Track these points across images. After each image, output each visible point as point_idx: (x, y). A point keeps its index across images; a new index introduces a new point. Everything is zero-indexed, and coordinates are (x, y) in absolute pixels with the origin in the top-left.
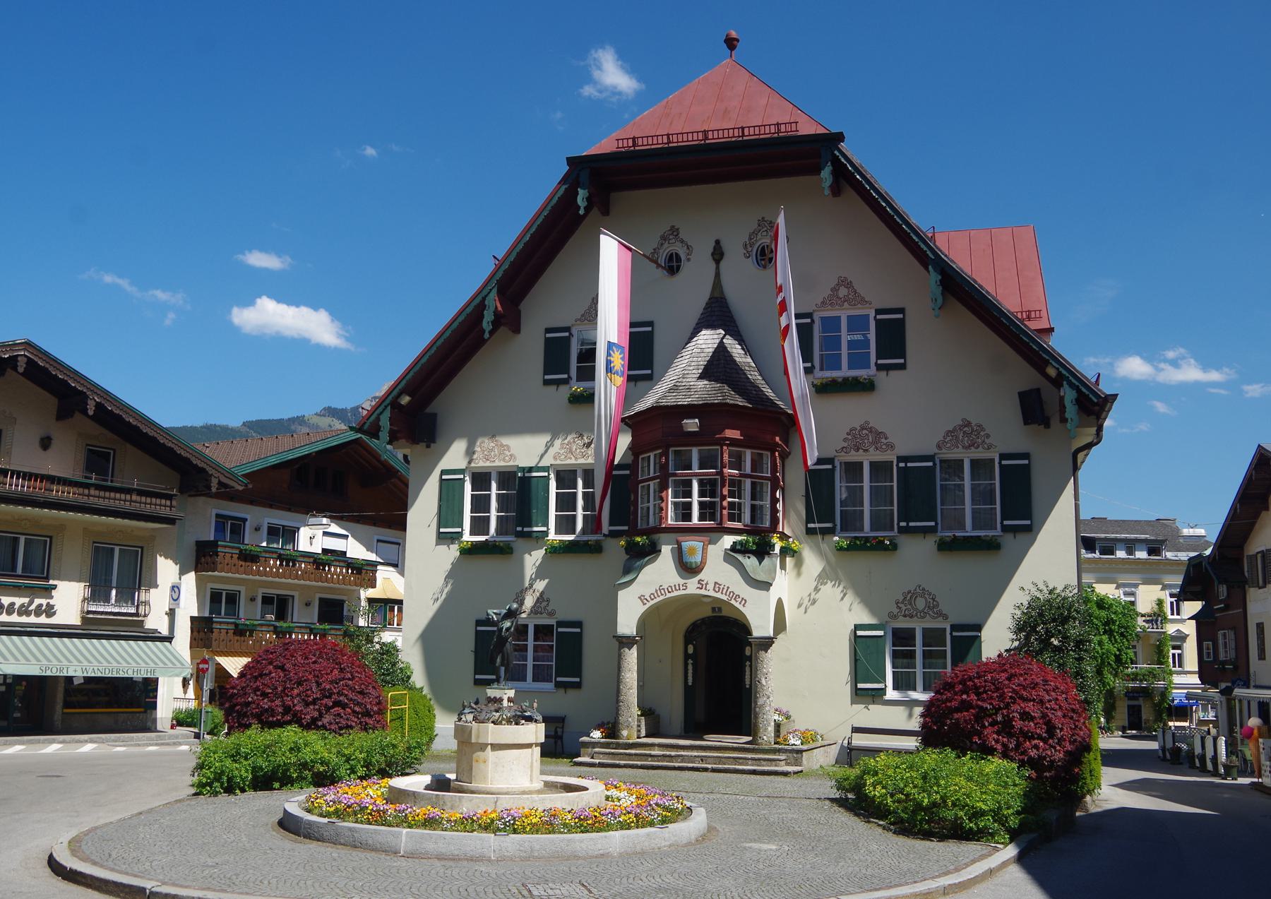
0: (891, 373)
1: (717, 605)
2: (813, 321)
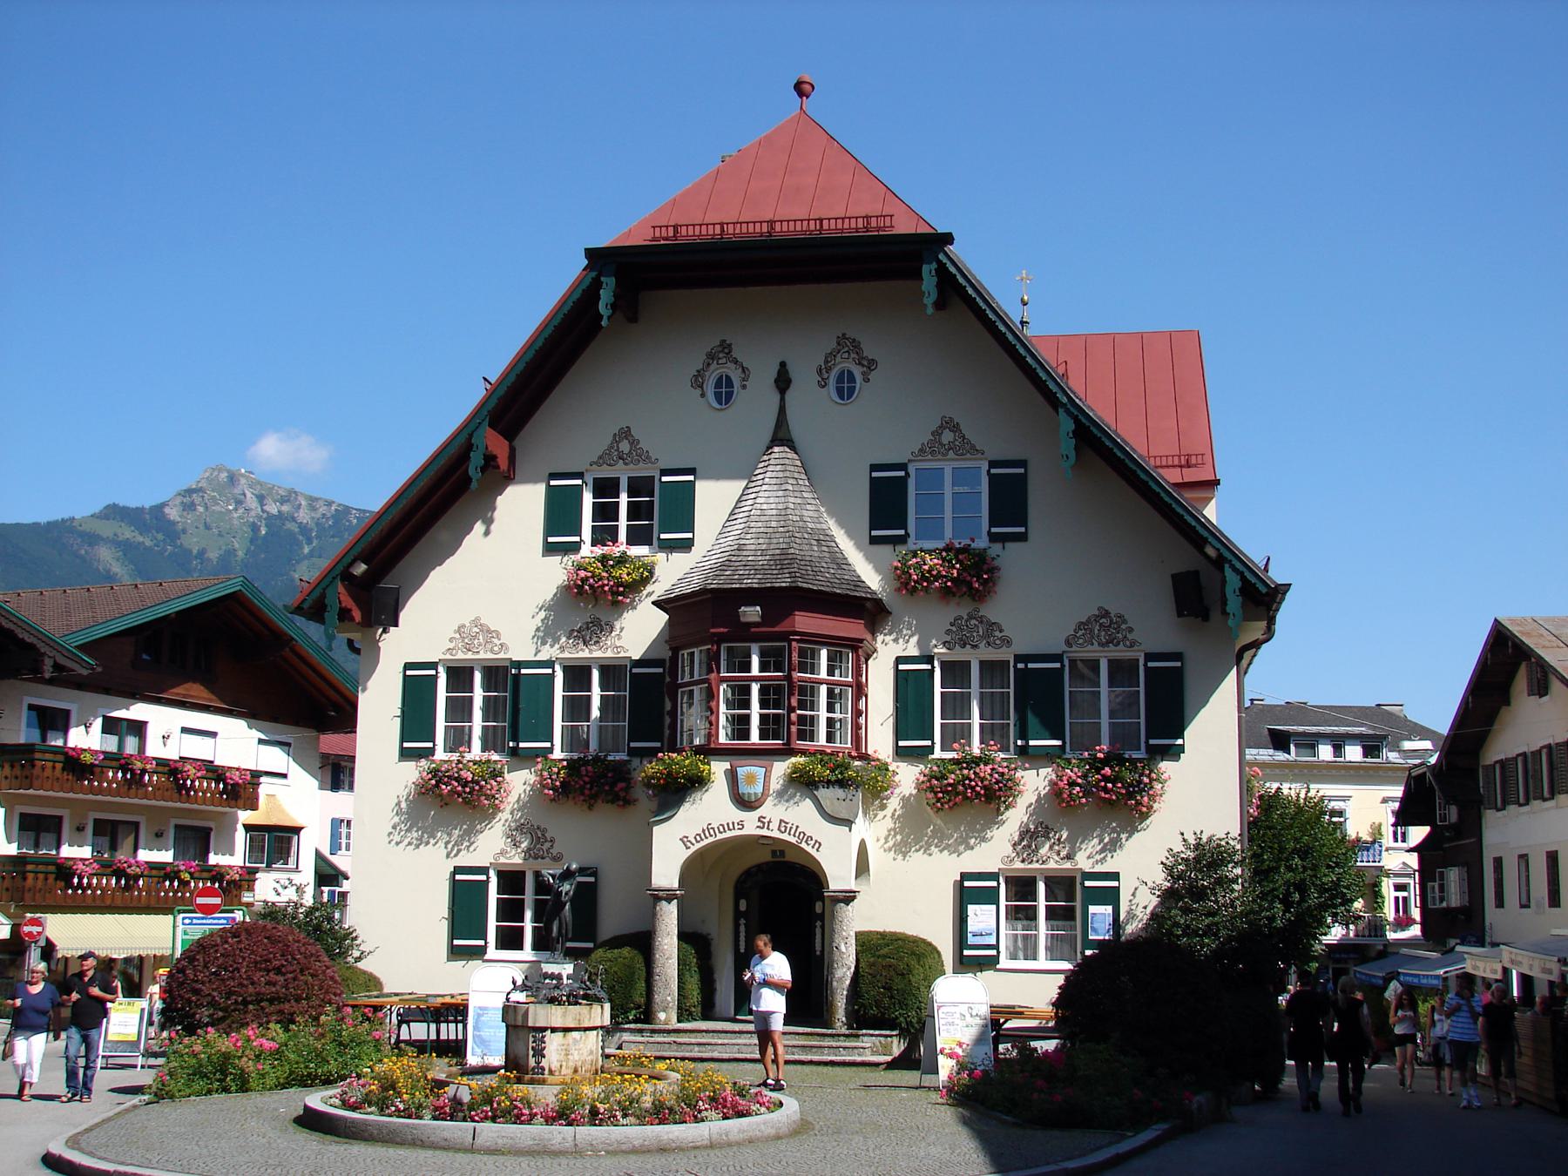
0: (1009, 545)
1: (778, 849)
2: (907, 474)
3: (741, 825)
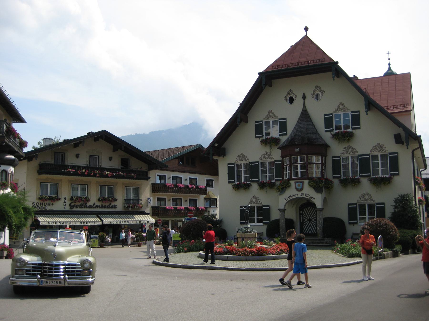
2: (333, 116)
3: (297, 195)
